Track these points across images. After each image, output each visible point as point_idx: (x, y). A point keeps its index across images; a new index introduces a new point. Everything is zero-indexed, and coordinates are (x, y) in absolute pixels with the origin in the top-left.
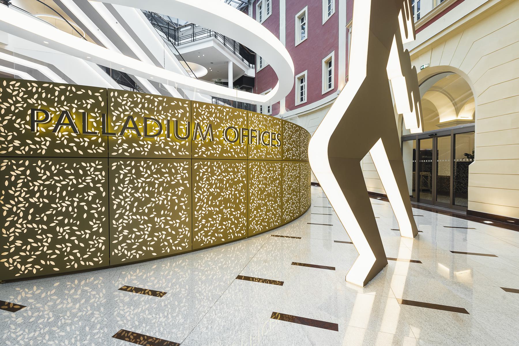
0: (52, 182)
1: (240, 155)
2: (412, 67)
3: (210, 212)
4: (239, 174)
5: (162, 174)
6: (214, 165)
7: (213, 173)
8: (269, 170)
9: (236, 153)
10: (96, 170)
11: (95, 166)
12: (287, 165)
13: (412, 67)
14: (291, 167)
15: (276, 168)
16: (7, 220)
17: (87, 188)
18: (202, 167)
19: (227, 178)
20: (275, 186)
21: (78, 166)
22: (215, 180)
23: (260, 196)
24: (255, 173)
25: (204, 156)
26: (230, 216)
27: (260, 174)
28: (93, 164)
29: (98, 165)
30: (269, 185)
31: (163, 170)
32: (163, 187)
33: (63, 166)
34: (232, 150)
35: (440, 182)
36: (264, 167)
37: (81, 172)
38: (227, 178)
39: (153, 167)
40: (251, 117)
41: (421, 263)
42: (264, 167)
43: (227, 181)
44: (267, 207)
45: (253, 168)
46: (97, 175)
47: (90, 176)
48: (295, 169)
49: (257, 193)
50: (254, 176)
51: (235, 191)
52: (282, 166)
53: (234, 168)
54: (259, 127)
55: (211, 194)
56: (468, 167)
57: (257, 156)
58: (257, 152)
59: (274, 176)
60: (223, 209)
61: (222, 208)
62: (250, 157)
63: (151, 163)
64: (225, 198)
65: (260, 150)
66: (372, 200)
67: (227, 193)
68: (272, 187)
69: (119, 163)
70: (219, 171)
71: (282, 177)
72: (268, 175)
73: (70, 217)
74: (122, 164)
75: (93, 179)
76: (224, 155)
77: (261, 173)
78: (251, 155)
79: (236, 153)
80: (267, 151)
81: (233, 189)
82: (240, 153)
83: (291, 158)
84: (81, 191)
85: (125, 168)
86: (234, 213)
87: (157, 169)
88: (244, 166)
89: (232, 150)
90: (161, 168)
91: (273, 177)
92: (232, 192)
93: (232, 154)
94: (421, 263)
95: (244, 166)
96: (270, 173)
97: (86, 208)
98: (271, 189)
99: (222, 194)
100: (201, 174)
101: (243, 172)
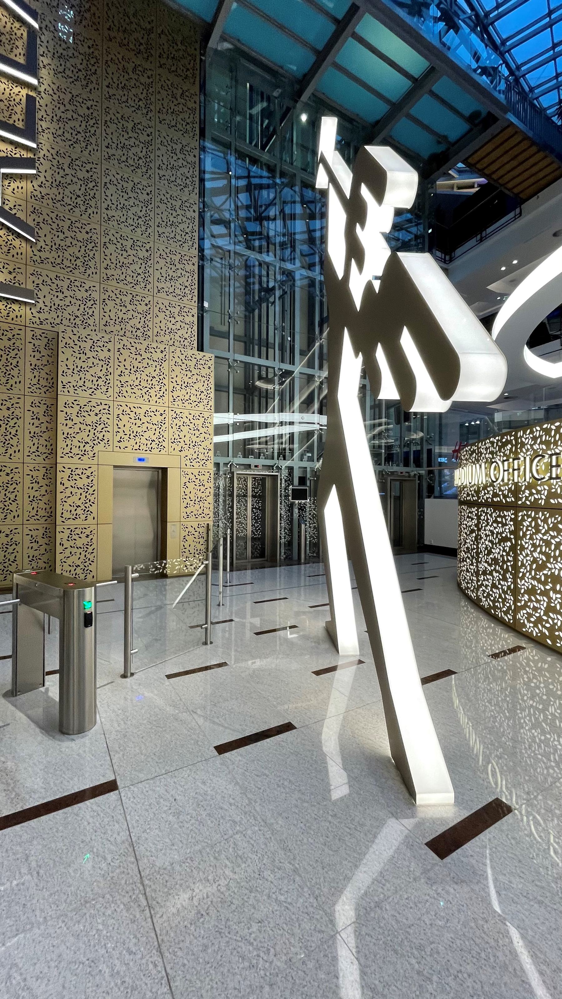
7: (538, 531)
12: (483, 511)
14: (491, 515)
19: (557, 540)
20: (504, 551)
23: (536, 574)
24: (527, 530)
25: (528, 503)
38: (557, 540)
40: (521, 437)
41: (314, 673)
45: (523, 520)
49: (531, 566)
50: (525, 535)
52: (516, 516)
54: (533, 449)
55: (535, 561)
57: (530, 501)
58: (531, 494)
62: (520, 502)
64: (553, 574)
70: (546, 526)
71: (517, 538)
76: (552, 501)
77: (538, 531)
78: (521, 499)
83: (490, 500)
94: (314, 673)
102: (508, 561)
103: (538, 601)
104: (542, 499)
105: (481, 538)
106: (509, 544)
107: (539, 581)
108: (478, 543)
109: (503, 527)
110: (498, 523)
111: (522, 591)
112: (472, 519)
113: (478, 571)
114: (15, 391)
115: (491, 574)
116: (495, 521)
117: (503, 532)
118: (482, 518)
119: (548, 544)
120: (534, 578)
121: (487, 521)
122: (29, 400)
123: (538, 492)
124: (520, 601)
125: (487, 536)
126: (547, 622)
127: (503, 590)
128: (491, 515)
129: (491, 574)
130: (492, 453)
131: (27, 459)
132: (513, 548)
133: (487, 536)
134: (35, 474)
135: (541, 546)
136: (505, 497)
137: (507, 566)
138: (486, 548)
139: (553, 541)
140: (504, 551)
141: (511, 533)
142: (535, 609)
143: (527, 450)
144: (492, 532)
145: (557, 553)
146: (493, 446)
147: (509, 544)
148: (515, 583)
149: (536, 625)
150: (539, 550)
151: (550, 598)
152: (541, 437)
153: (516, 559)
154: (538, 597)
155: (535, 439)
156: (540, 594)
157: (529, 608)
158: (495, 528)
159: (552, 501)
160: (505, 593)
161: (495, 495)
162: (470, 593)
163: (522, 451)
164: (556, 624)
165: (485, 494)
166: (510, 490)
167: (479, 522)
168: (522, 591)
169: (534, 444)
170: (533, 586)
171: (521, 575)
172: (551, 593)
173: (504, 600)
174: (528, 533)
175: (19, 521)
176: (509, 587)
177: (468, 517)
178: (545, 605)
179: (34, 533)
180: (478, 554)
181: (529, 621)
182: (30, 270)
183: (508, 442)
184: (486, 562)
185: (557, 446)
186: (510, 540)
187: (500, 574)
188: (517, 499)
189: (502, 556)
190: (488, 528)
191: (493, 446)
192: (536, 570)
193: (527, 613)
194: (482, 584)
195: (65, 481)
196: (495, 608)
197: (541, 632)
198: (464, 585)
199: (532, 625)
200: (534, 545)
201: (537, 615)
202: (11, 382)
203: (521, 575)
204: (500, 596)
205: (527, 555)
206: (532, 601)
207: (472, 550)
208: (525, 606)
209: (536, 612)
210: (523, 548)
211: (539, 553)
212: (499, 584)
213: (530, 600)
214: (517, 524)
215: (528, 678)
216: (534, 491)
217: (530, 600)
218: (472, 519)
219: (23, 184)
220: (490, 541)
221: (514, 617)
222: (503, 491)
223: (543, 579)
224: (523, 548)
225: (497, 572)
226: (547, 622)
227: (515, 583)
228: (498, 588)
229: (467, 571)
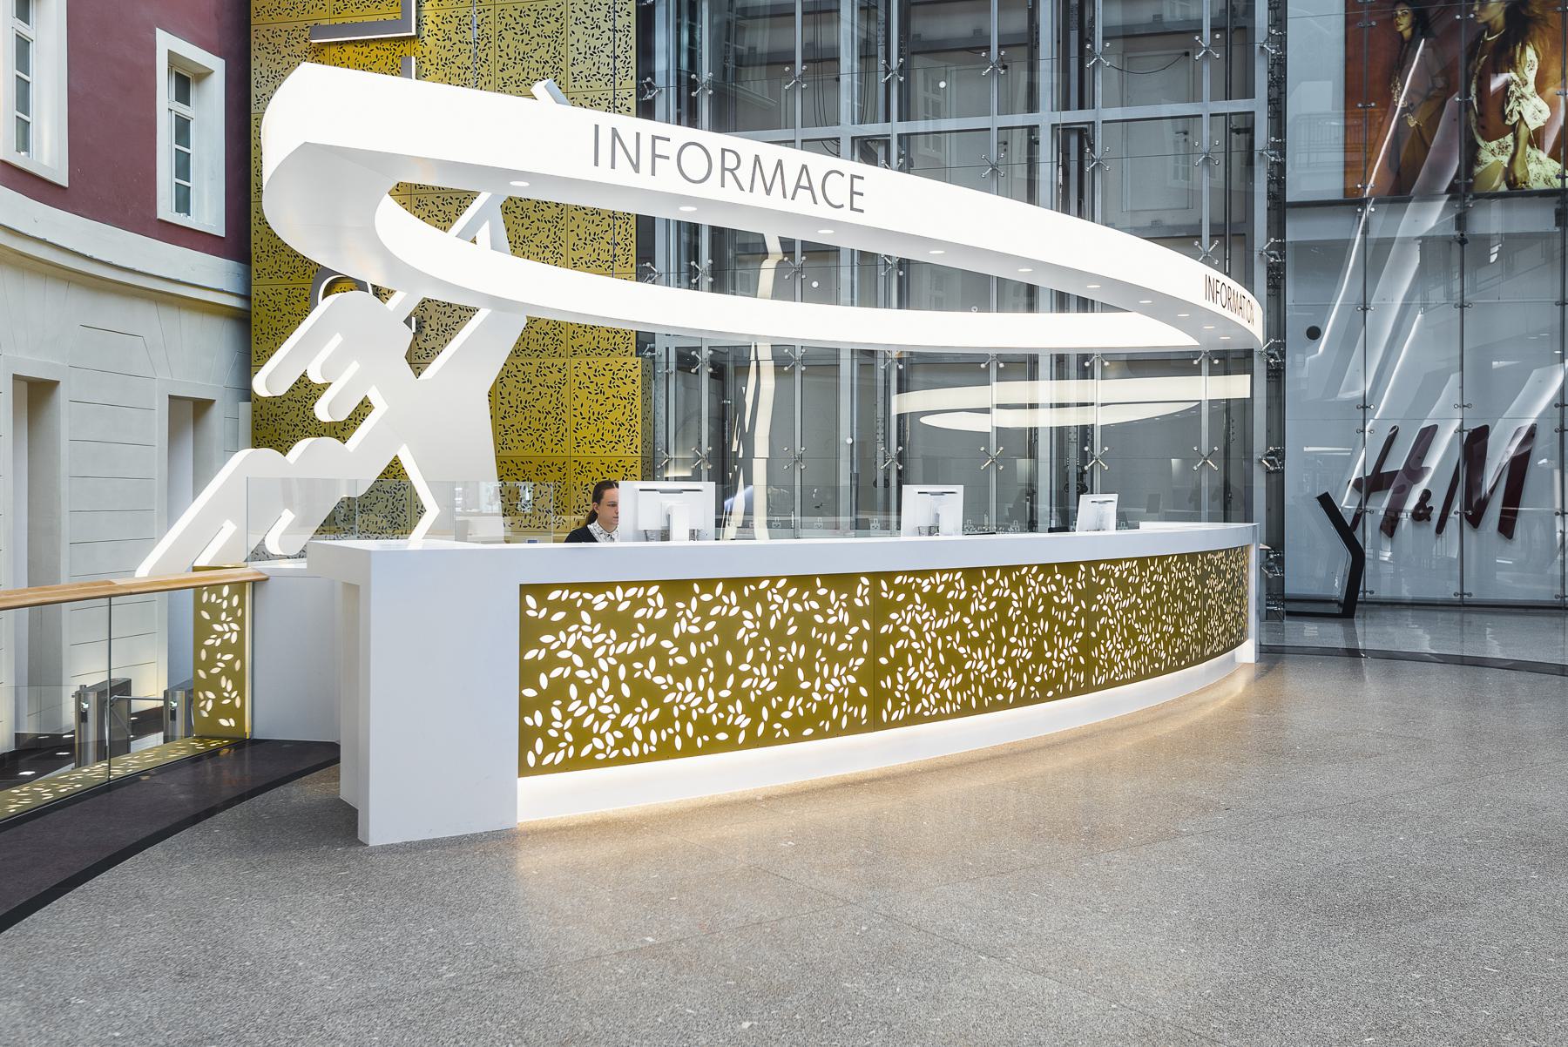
26: (828, 595)
30: (839, 699)
35: (474, 242)
44: (1074, 584)
51: (812, 689)
56: (291, 67)
60: (850, 626)
61: (854, 630)
64: (844, 663)
66: (1383, 471)
67: (836, 682)
68: (1059, 660)
81: (817, 697)
86: (815, 605)
89: (822, 592)
92: (822, 686)
98: (1060, 651)
99: (852, 679)
185: (836, 693)
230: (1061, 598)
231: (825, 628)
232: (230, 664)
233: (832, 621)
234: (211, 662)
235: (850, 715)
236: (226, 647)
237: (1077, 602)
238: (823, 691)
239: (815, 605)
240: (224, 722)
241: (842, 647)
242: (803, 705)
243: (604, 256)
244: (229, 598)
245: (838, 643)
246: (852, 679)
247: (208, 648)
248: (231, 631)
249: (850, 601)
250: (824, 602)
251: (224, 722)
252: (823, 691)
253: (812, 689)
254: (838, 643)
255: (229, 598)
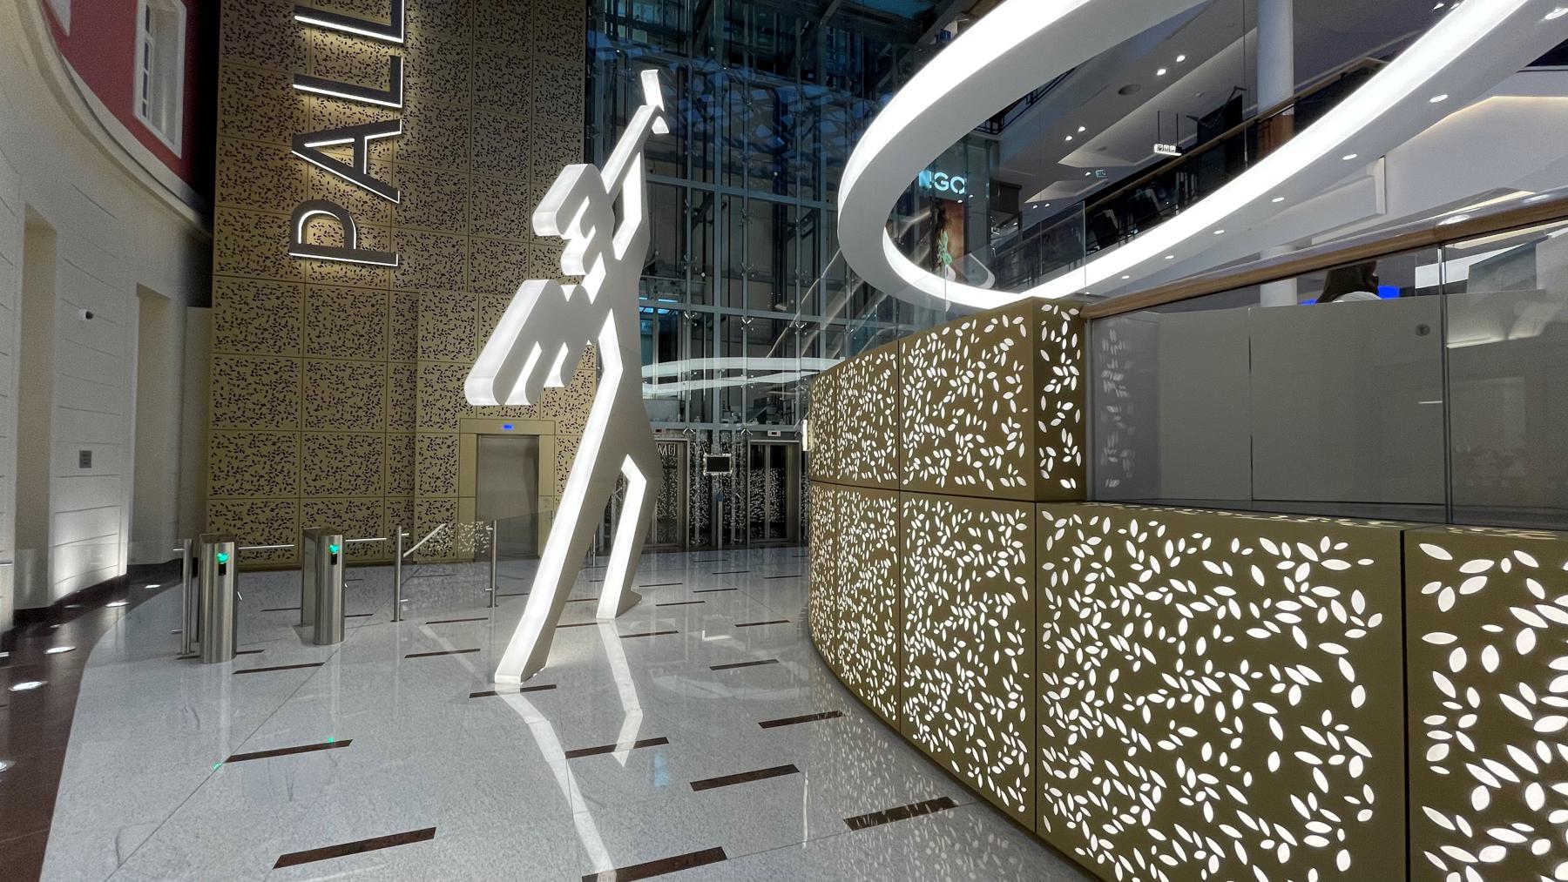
0: (1165, 594)
1: (1004, 481)
2: (593, 231)
3: (1112, 734)
4: (1003, 555)
5: (1207, 583)
6: (1128, 536)
7: (1125, 574)
8: (963, 535)
9: (992, 473)
10: (1319, 575)
11: (1315, 558)
12: (844, 497)
13: (593, 231)
14: (857, 506)
15: (998, 535)
16: (1459, 819)
17: (1282, 651)
18: (1081, 536)
19: (1200, 607)
20: (880, 576)
21: (1248, 551)
22: (1133, 604)
27: (932, 545)
28: (1305, 549)
29: (1332, 554)
31: (1211, 566)
32: (1209, 639)
33: (1197, 543)
34: (978, 464)
36: (946, 520)
37: (1258, 576)
39: (1169, 548)
42: (946, 520)
43: (1201, 624)
45: (912, 517)
46: (1324, 602)
47: (1294, 597)
48: (874, 521)
49: (925, 608)
50: (914, 547)
51: (986, 372)
52: (900, 510)
53: (984, 528)
55: (931, 599)
58: (924, 466)
59: (988, 567)
61: (1056, 422)
63: (1161, 531)
65: (932, 457)
69: (1506, 565)
72: (961, 554)
73: (1221, 744)
74: (1531, 572)
75: (1307, 615)
77: (1125, 574)
79: (992, 473)
80: (953, 460)
81: (982, 365)
82: (1003, 472)
84: (1263, 654)
85: (1087, 537)
86: (984, 452)
87: (1183, 555)
88: (1021, 527)
89: (978, 464)
90: (1202, 556)
91: (982, 570)
93: (977, 478)
95: (1021, 527)
96: (970, 547)
97: (1277, 730)
100: (1077, 567)
101: (1016, 551)
102: (887, 597)
103: (937, 682)
104: (940, 475)
105: (842, 549)
106: (887, 563)
107: (1133, 720)
108: (837, 558)
109: (876, 529)
110: (869, 521)
111: (912, 659)
112: (828, 512)
113: (837, 611)
114: (378, 358)
115: (858, 619)
116: (864, 518)
117: (877, 541)
118: (843, 510)
119: (1165, 616)
120: (929, 634)
121: (850, 516)
122: (392, 367)
123: (936, 462)
124: (908, 679)
125: (850, 545)
126: (952, 726)
127: (879, 653)
128: (857, 506)
129: (858, 619)
130: (858, 387)
131: (390, 429)
132: (896, 571)
133: (850, 545)
134: (397, 444)
135: (941, 571)
136: (882, 470)
137: (886, 607)
138: (850, 569)
139: (1181, 608)
140: (880, 576)
141: (891, 541)
142: (1123, 803)
143: (917, 380)
144: (858, 537)
145: (1201, 646)
146: (859, 374)
147: (887, 563)
148: (899, 641)
149: (933, 732)
150: (1129, 629)
151: (956, 678)
152: (939, 352)
153: (900, 596)
154: (1128, 766)
155: (929, 357)
156: (1135, 761)
157: (1098, 791)
158: (865, 531)
159: (957, 479)
160: (883, 660)
161: (864, 467)
162: (826, 652)
163: (908, 382)
164: (1204, 864)
165: (847, 465)
166: (888, 457)
167: (837, 519)
168: (912, 659)
169: (928, 367)
170: (929, 650)
171: (908, 626)
172: (1180, 766)
173: (881, 673)
174: (1091, 577)
175: (380, 493)
176: (888, 648)
177: (822, 507)
178: (1157, 795)
179: (396, 506)
180: (837, 578)
181: (924, 722)
182: (395, 231)
183: (886, 365)
184: (849, 595)
185: (966, 369)
186: (889, 555)
187: (872, 619)
188: (902, 475)
189: (877, 586)
190: (938, 550)
191: (859, 374)
192: (934, 618)
193: (920, 704)
194: (843, 638)
195: (424, 451)
196: (866, 687)
197: (942, 744)
198: (816, 634)
199: (1108, 845)
200: (929, 568)
201: (936, 709)
202: (375, 349)
203: (908, 626)
204: (874, 666)
205: (918, 587)
206: (1106, 775)
207: (829, 569)
208: (916, 690)
209: (934, 703)
210: (912, 574)
211: (1130, 640)
212: (873, 640)
213: (924, 679)
214: (902, 524)
215: (922, 836)
216: (928, 460)
217: (924, 679)
218: (828, 512)
219: (390, 145)
220: (856, 556)
221: (899, 708)
222: (876, 460)
223: (1147, 715)
224: (912, 574)
225: (868, 616)
226: (952, 726)
227: (899, 641)
228: (871, 650)
229: (821, 609)
230: (974, 440)
231: (975, 430)
232: (1070, 414)
233: (969, 437)
234: (1052, 412)
235: (1059, 334)
236: (1066, 394)
237: (951, 435)
238: (976, 371)
239: (984, 452)
240: (1065, 484)
241: (961, 412)
242: (994, 356)
243: (433, 219)
244: (1069, 337)
245: (964, 415)
246: (1057, 370)
247: (1048, 395)
248: (1071, 375)
249: (955, 455)
250: (976, 455)
251: (1065, 484)
252: (976, 371)
253: (986, 372)
254: (964, 415)
255: (1069, 337)
